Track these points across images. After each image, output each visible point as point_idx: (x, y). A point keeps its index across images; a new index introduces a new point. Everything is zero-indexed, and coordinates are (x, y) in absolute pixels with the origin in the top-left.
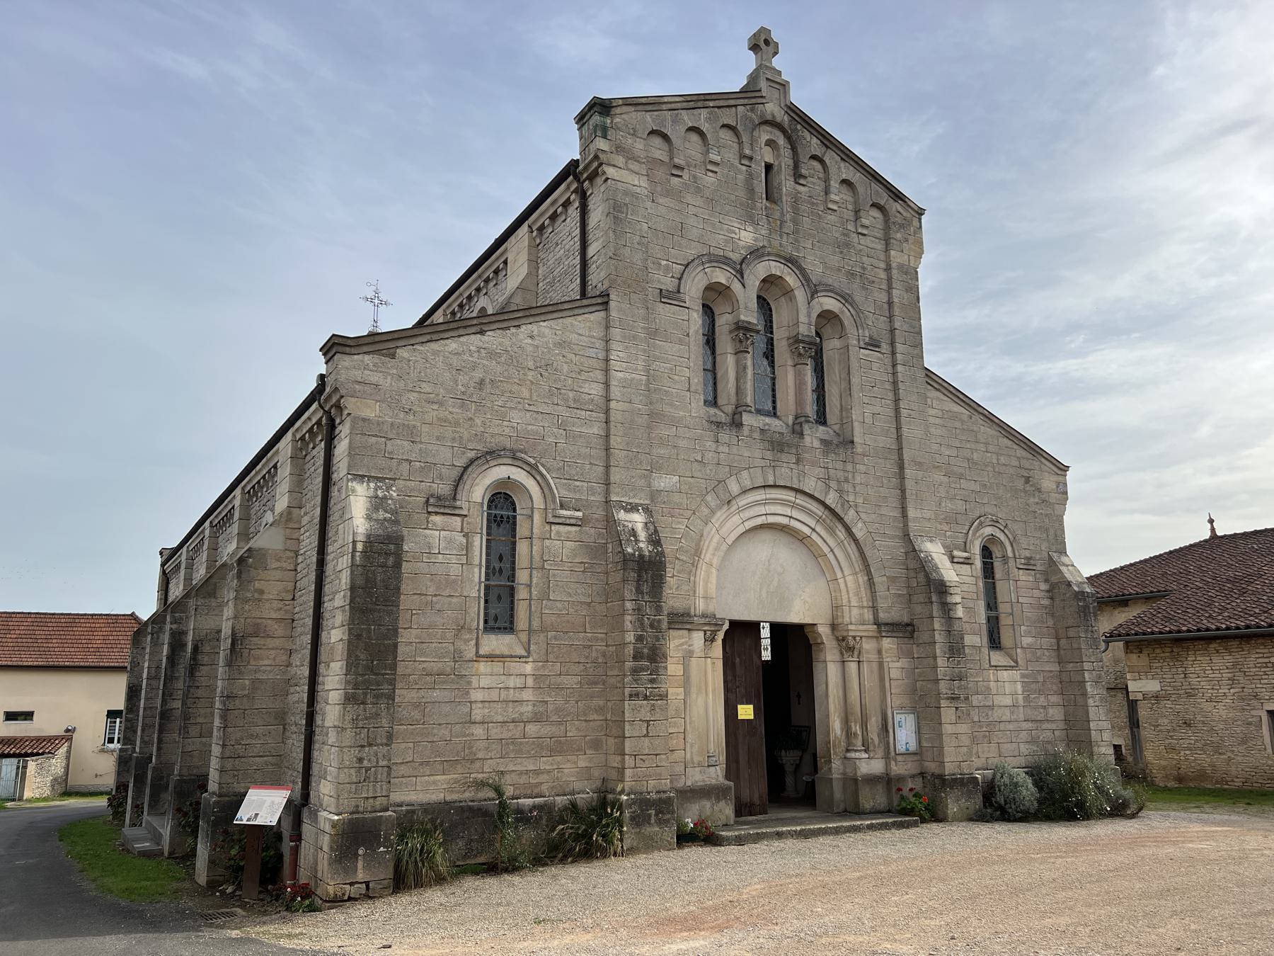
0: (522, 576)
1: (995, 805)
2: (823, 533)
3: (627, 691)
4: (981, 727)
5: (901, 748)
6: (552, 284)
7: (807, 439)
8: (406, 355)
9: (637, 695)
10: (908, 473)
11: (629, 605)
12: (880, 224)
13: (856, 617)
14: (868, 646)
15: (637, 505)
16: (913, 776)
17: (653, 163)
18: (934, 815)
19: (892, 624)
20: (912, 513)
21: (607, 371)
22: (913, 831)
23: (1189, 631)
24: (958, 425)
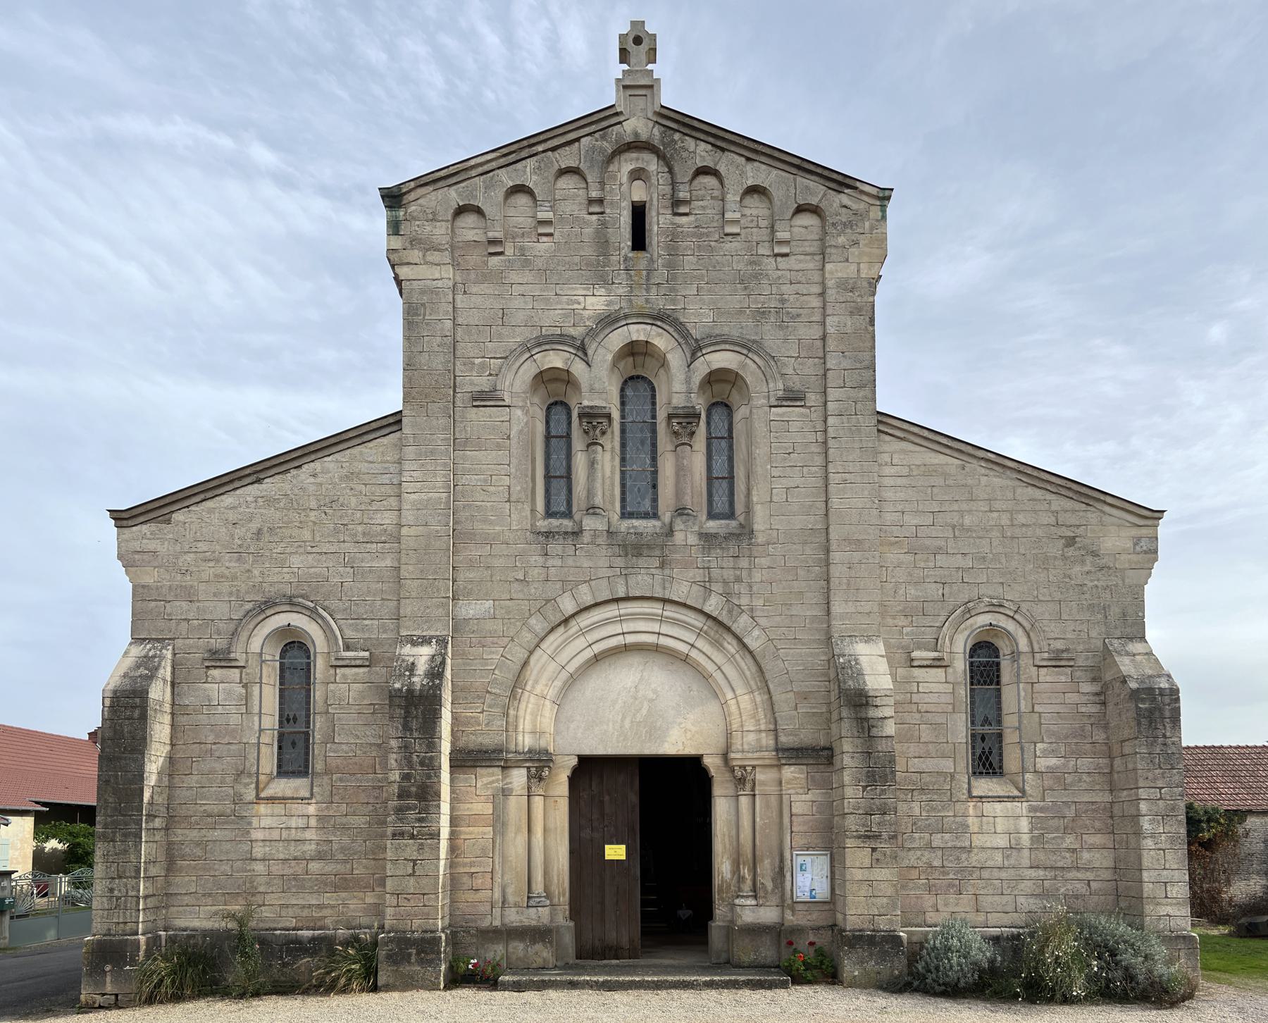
2: (707, 648)
3: (390, 831)
4: (945, 873)
10: (836, 556)
11: (394, 743)
15: (432, 637)
19: (797, 749)
20: (837, 608)
24: (939, 481)
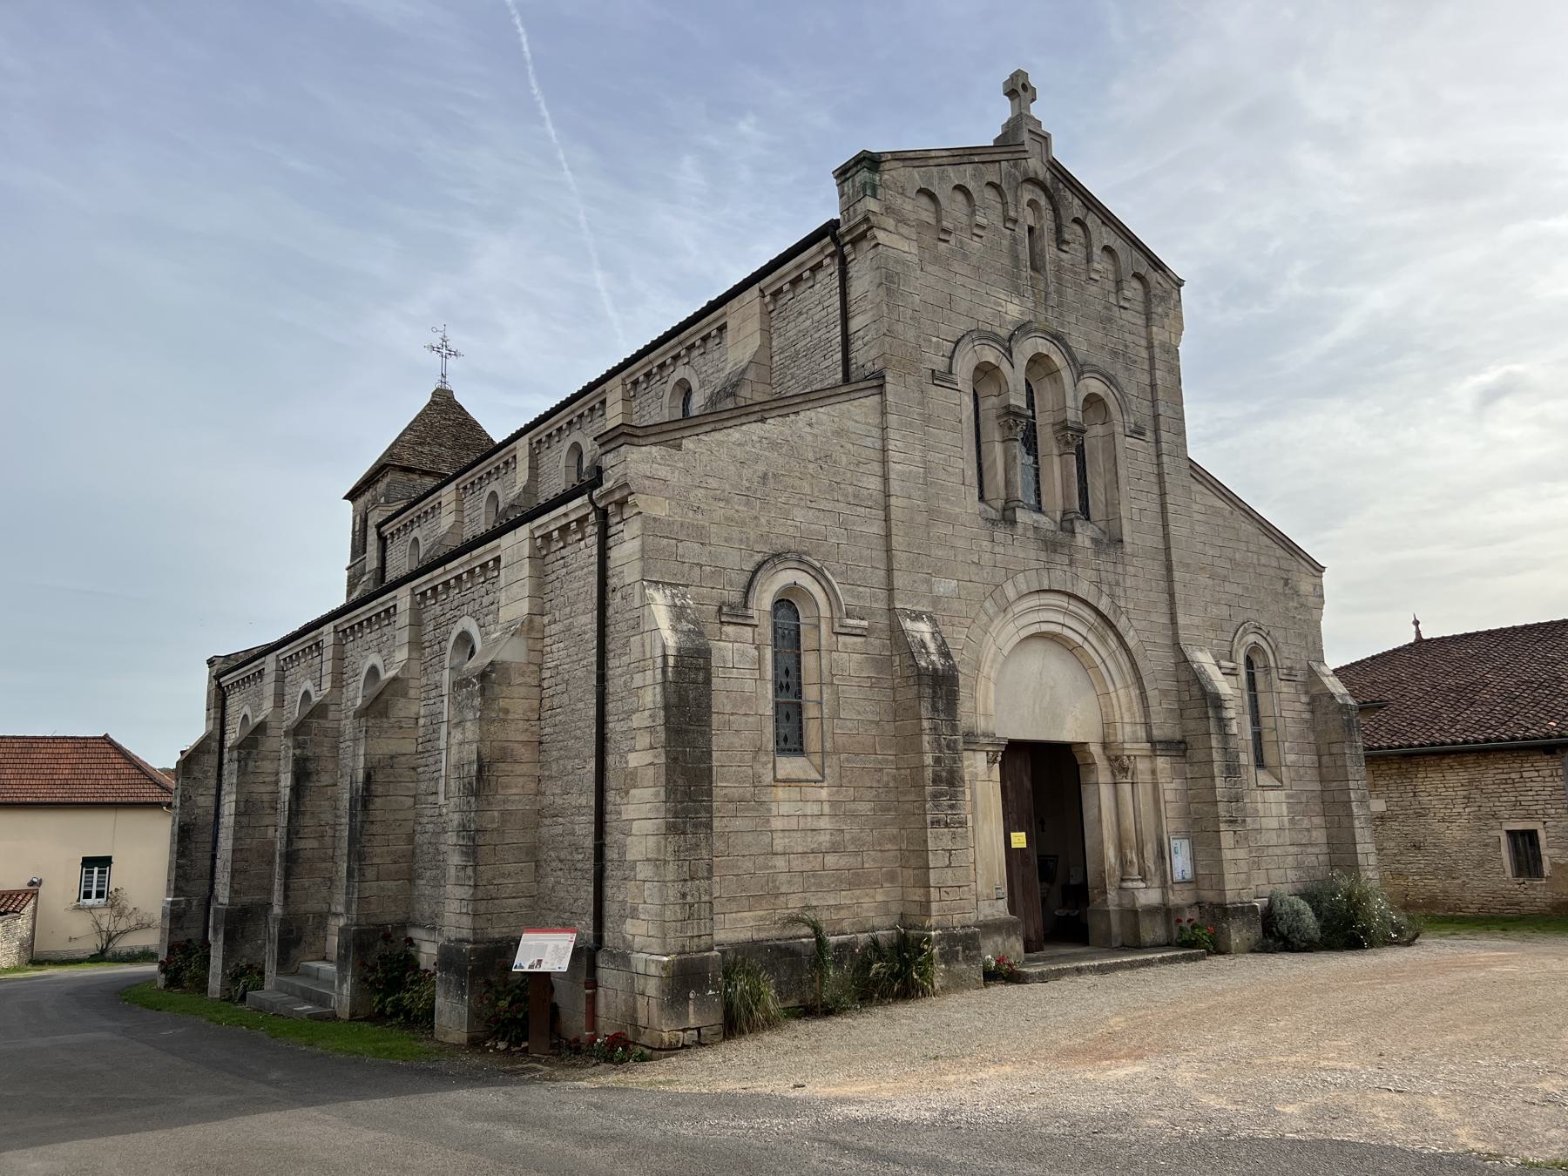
0: (810, 693)
1: (1276, 934)
2: (1094, 642)
5: (1178, 876)
6: (795, 358)
7: (1079, 538)
8: (691, 446)
9: (938, 822)
10: (1177, 575)
12: (1140, 296)
13: (1129, 734)
14: (1142, 766)
16: (1190, 906)
17: (922, 225)
18: (1218, 948)
20: (1182, 620)
21: (884, 462)
22: (1203, 964)
23: (1421, 745)
24: (1221, 522)
